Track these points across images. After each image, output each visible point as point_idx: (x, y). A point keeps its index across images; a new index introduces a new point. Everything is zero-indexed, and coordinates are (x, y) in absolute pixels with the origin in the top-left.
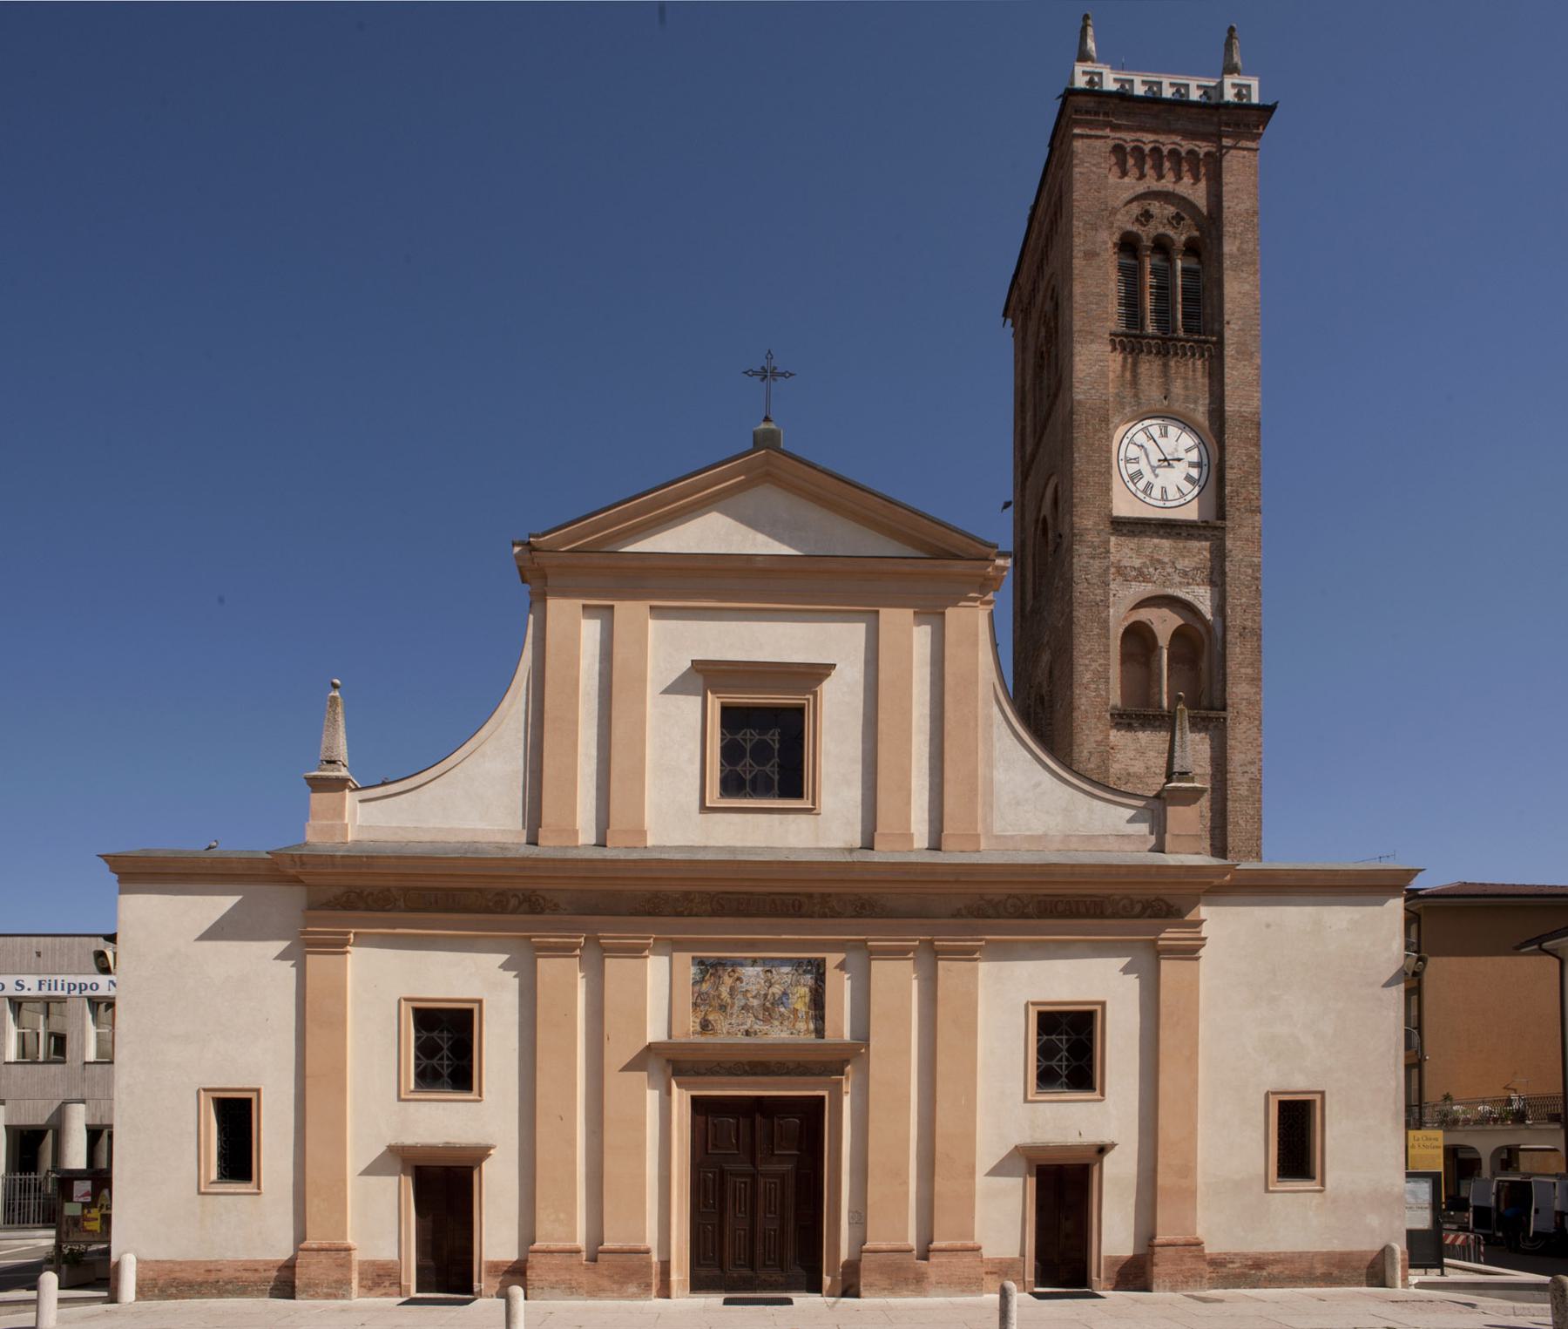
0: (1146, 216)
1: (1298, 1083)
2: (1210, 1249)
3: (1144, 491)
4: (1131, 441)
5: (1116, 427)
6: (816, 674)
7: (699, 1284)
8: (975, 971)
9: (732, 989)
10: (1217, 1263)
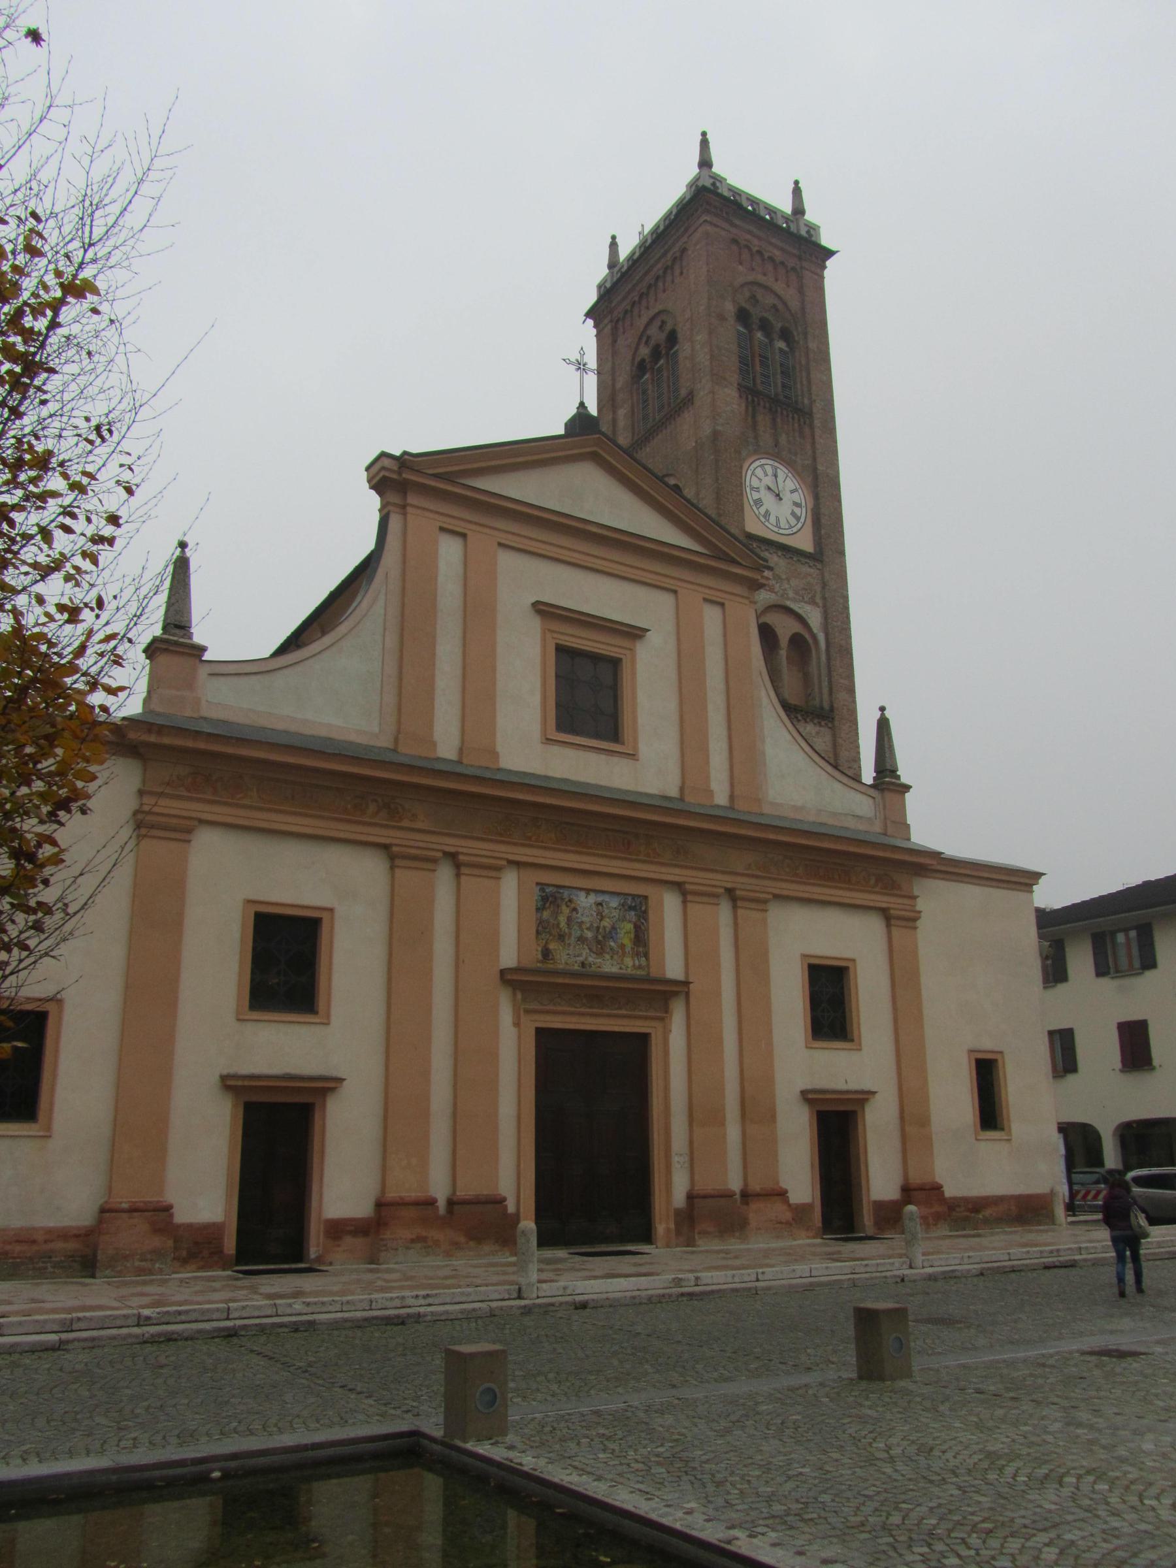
0: (753, 299)
1: (987, 1044)
2: (949, 1192)
3: (765, 516)
4: (753, 473)
5: (744, 460)
6: (635, 634)
7: (545, 1241)
8: (519, 962)
9: (569, 919)
10: (953, 1205)
